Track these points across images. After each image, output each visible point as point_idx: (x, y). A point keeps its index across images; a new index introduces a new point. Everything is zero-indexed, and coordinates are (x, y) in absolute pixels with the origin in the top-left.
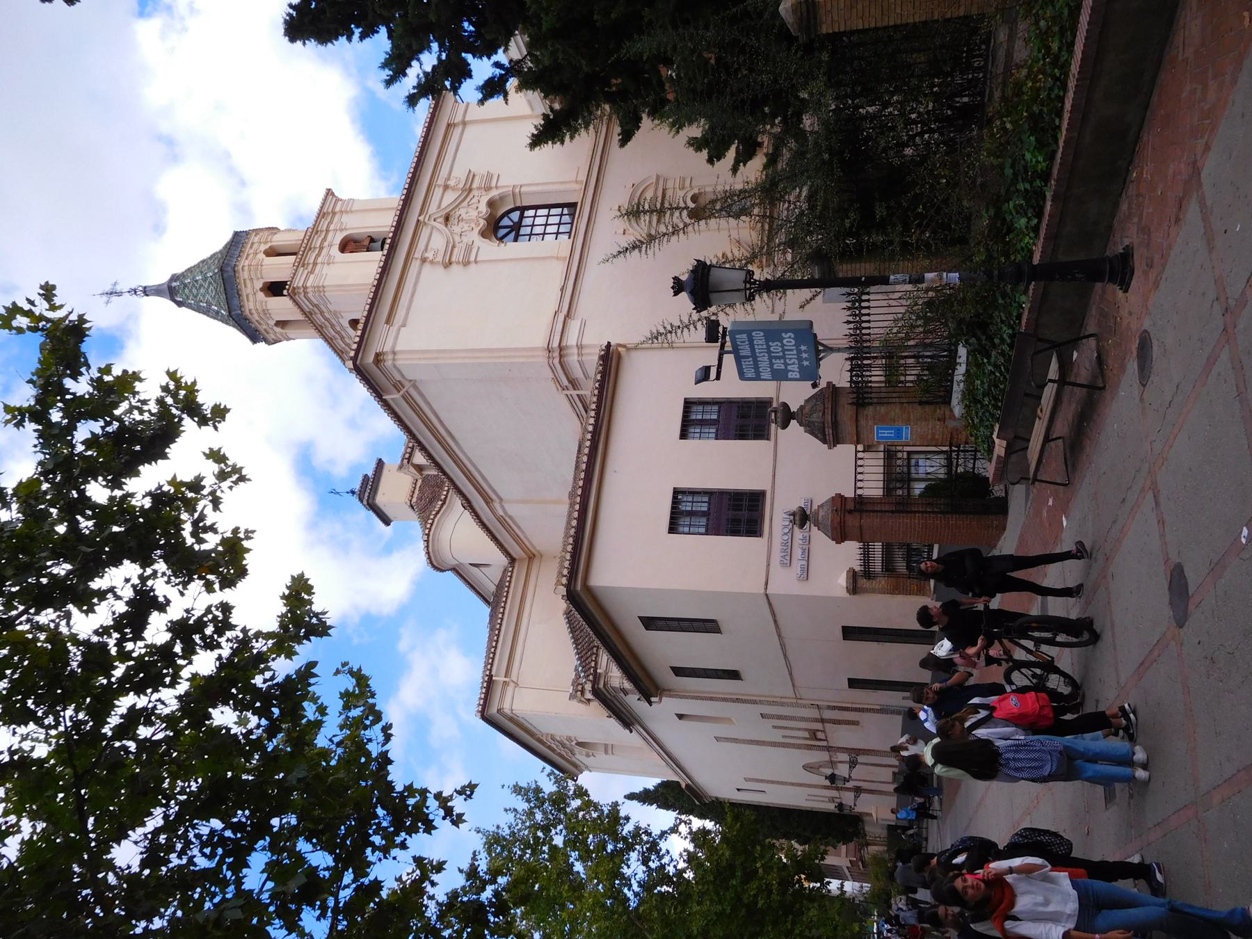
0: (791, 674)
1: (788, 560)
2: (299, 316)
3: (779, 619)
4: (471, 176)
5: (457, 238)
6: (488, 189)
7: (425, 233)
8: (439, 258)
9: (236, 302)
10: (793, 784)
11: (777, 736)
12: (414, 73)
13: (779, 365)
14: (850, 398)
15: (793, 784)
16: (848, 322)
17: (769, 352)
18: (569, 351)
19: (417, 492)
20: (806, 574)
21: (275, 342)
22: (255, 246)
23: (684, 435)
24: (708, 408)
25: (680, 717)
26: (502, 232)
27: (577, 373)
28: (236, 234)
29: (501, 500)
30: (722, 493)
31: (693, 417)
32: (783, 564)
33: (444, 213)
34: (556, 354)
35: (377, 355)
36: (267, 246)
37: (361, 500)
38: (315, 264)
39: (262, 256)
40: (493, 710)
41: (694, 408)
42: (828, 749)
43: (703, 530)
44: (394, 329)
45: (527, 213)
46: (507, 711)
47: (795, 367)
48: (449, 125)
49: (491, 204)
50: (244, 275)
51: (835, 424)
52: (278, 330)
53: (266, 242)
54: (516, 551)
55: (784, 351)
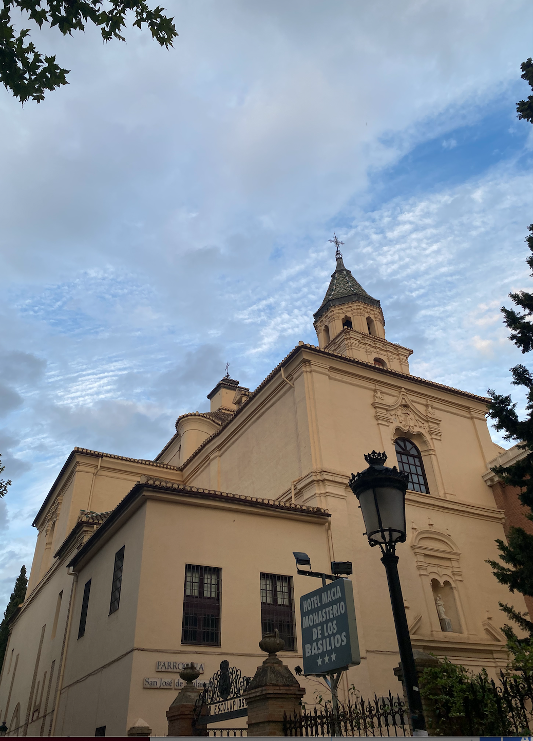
0: (77, 682)
1: (162, 669)
2: (332, 337)
3: (116, 664)
4: (437, 422)
5: (393, 413)
6: (430, 433)
7: (395, 393)
8: (377, 401)
9: (337, 303)
10: (10, 696)
11: (40, 677)
12: (520, 310)
13: (316, 633)
14: (290, 715)
15: (10, 696)
16: (362, 703)
17: (327, 622)
18: (322, 487)
19: (229, 412)
20: (149, 687)
21: (316, 327)
22: (372, 312)
23: (264, 576)
24: (286, 596)
25: (61, 594)
26: (402, 444)
27: (307, 495)
28: (379, 302)
29: (220, 456)
30: (218, 609)
31: (278, 584)
32: (159, 664)
33: (409, 403)
34: (319, 478)
35: (309, 361)
36: (373, 318)
37: (223, 380)
38: (365, 344)
39: (367, 315)
40: (78, 459)
41: (285, 584)
42: (27, 725)
43: (188, 593)
44: (327, 372)
45: (417, 460)
46: (78, 468)
47: (315, 651)
48: (469, 408)
49: (420, 435)
50: (354, 306)
51: (265, 698)
52: (323, 328)
53: (375, 318)
54: (188, 471)
55: (329, 636)
